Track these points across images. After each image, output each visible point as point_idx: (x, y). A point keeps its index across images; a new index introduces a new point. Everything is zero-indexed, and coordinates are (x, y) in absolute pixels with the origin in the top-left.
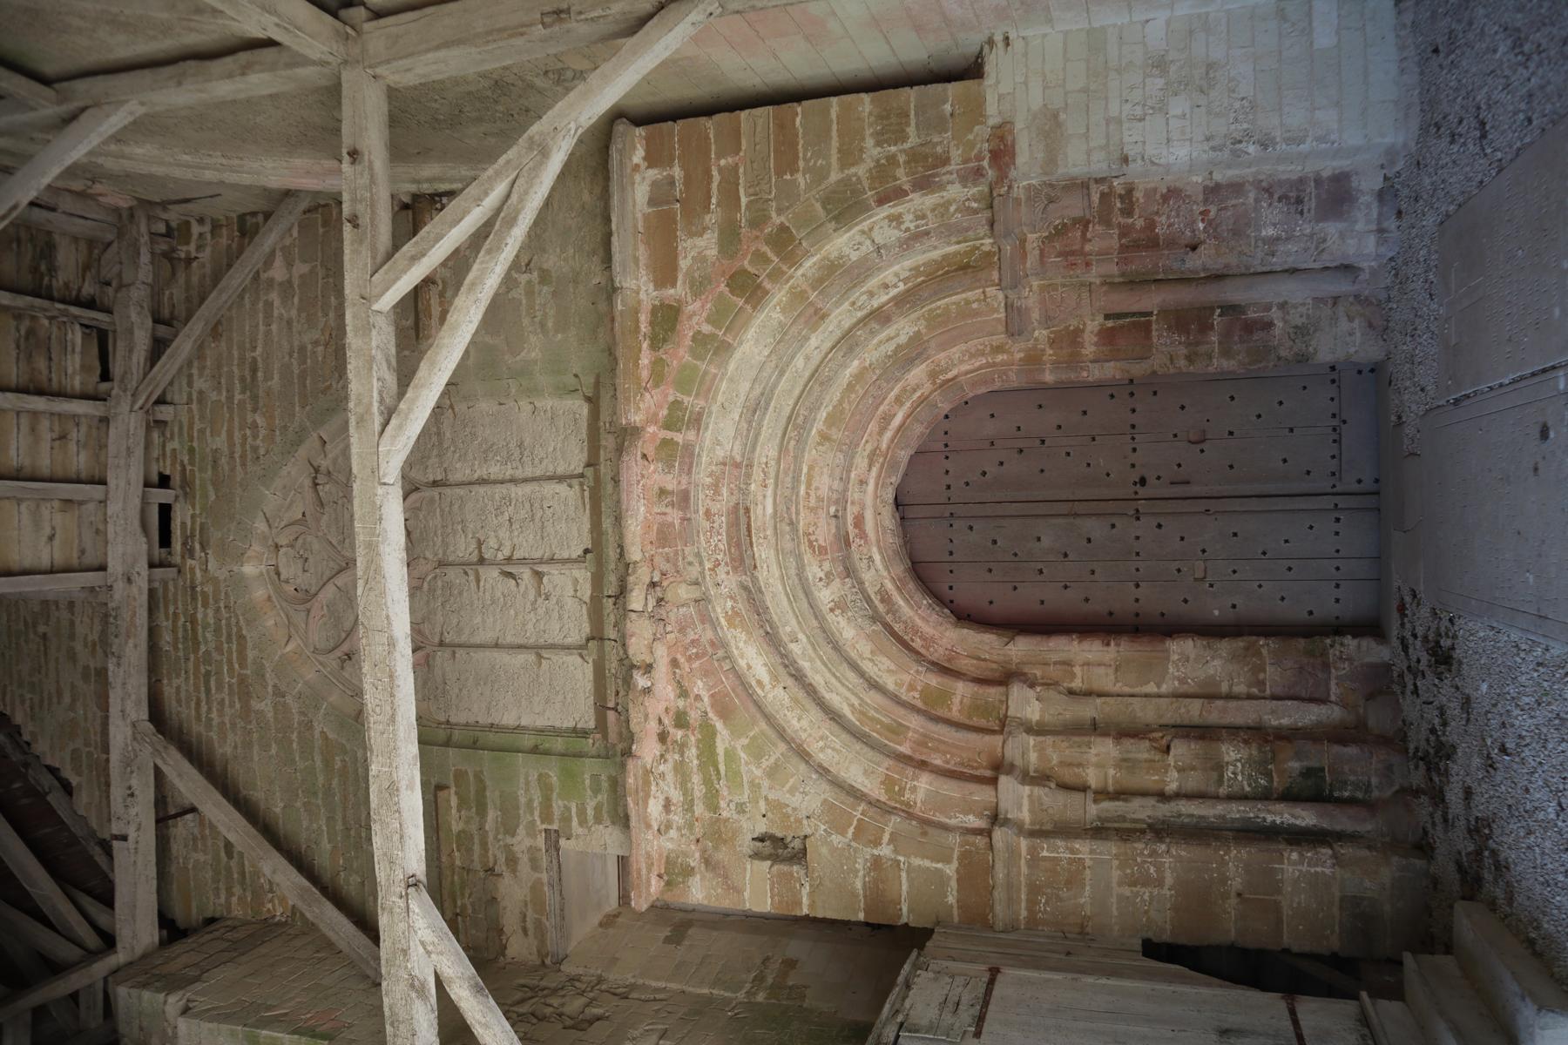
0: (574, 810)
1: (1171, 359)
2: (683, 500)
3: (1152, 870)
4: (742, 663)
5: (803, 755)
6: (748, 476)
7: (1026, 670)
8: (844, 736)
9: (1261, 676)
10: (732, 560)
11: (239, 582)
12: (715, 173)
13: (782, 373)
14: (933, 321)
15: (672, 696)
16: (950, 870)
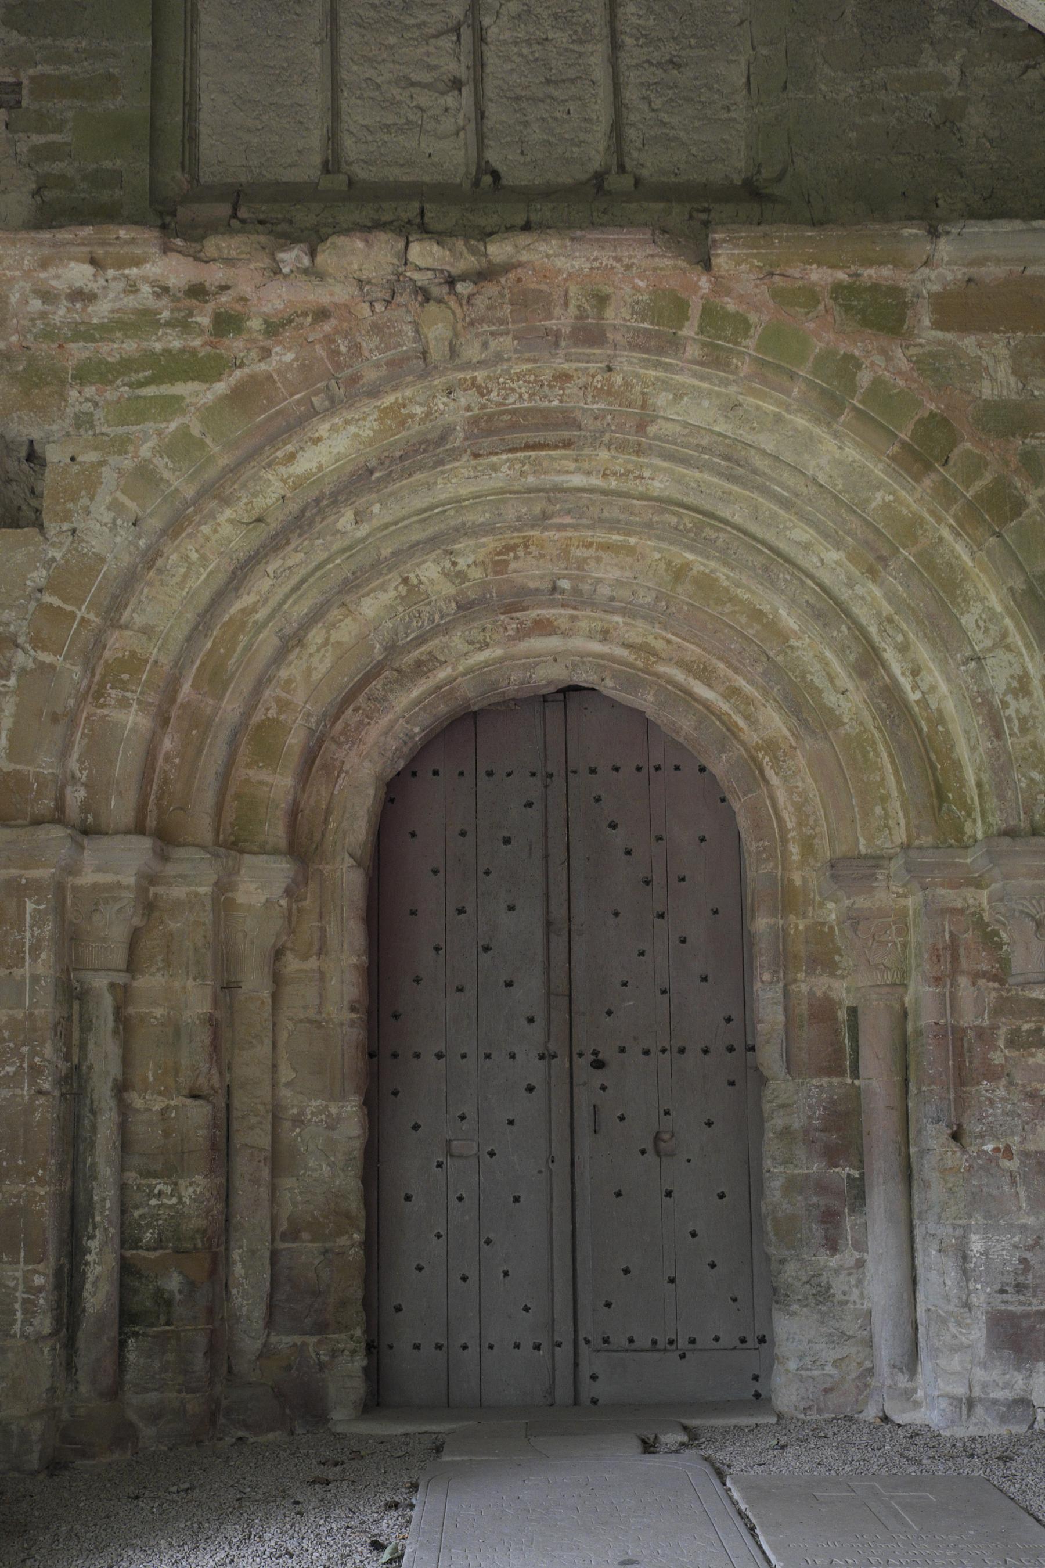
1: (784, 1106)
2: (590, 335)
3: (10, 1069)
4: (323, 429)
5: (176, 526)
6: (622, 447)
7: (312, 885)
8: (205, 597)
9: (305, 1236)
10: (490, 417)
13: (786, 504)
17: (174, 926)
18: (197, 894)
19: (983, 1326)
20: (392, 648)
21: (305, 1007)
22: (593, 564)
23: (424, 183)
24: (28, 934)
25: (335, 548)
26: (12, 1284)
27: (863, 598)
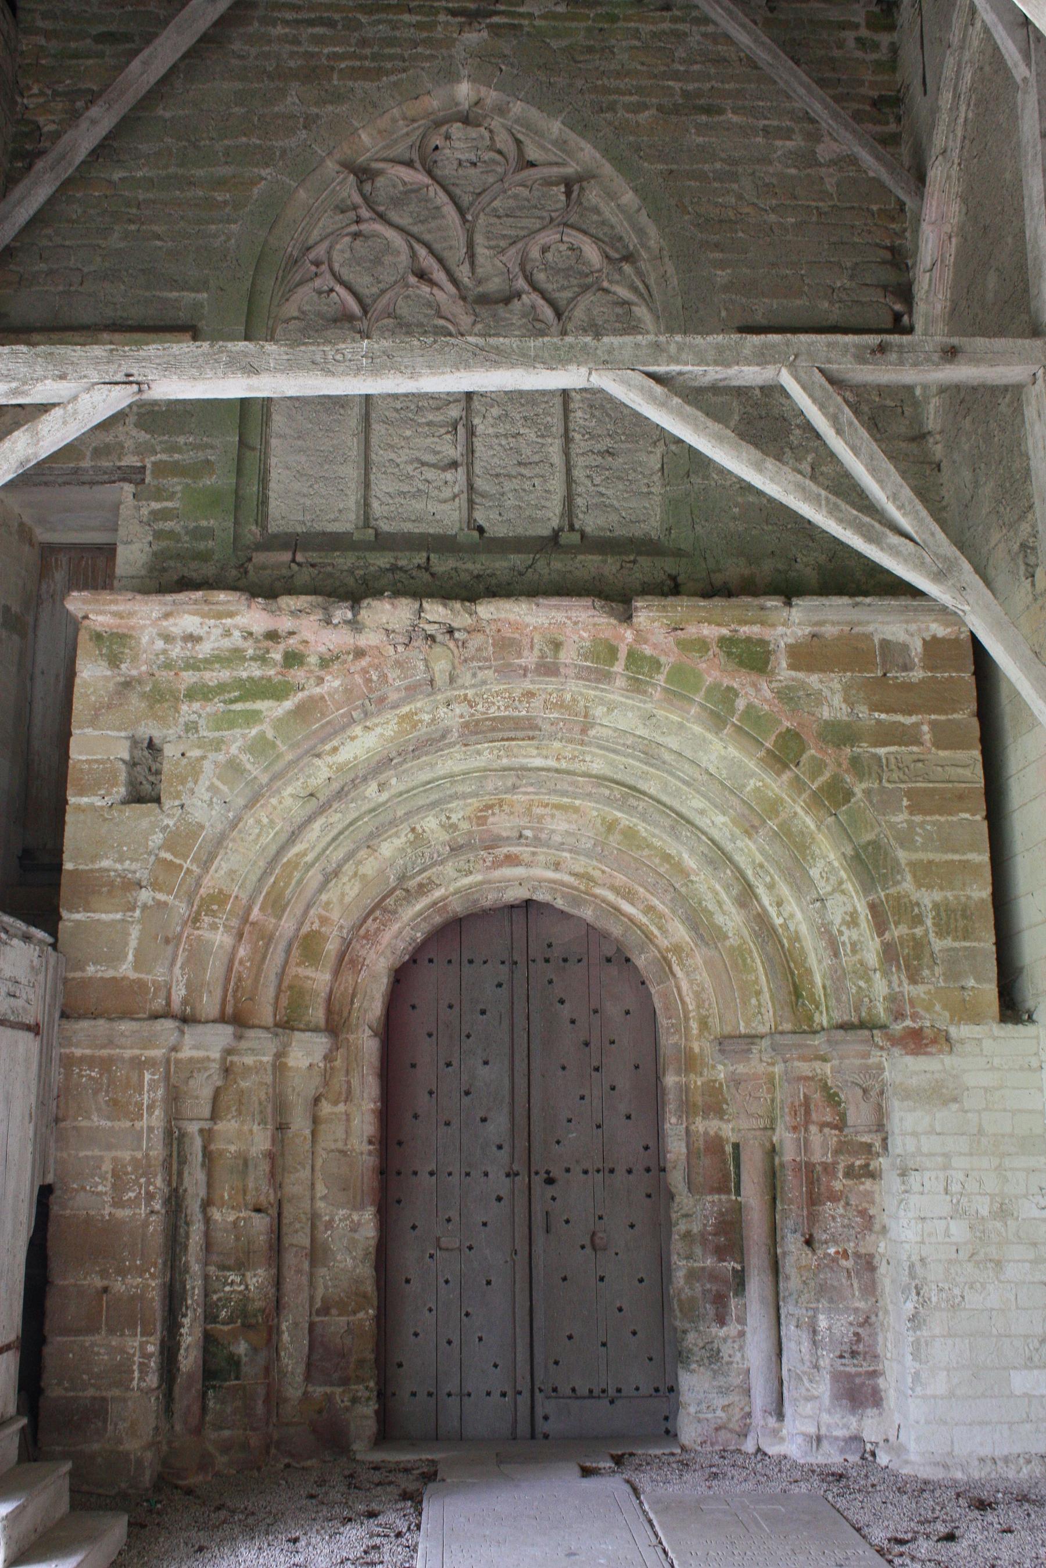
0: (169, 504)
1: (686, 1216)
2: (548, 669)
3: (132, 1195)
4: (358, 730)
8: (273, 849)
9: (334, 1311)
10: (477, 722)
11: (451, 76)
13: (684, 782)
14: (739, 953)
15: (322, 649)
16: (126, 969)
17: (244, 1084)
18: (261, 1062)
19: (828, 1381)
20: (402, 878)
21: (336, 1141)
22: (548, 819)
23: (429, 534)
24: (146, 1097)
25: (364, 809)
26: (132, 1351)
27: (742, 850)
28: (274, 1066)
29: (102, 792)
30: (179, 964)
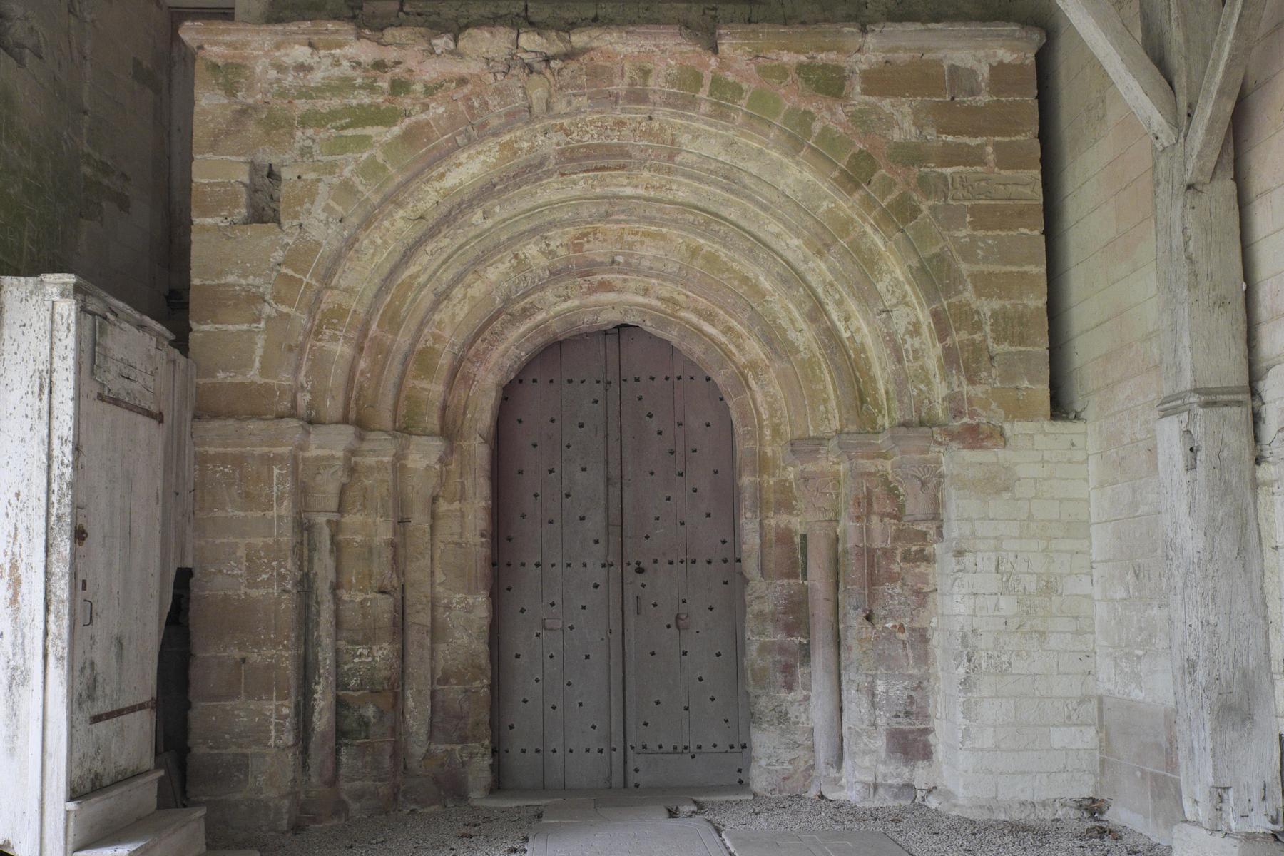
2: (637, 96)
3: (265, 576)
4: (463, 157)
7: (455, 455)
8: (387, 268)
9: (453, 681)
10: (572, 150)
12: (979, 140)
16: (253, 375)
17: (367, 482)
20: (507, 301)
22: (638, 246)
28: (394, 465)
29: (225, 213)
30: (303, 373)
